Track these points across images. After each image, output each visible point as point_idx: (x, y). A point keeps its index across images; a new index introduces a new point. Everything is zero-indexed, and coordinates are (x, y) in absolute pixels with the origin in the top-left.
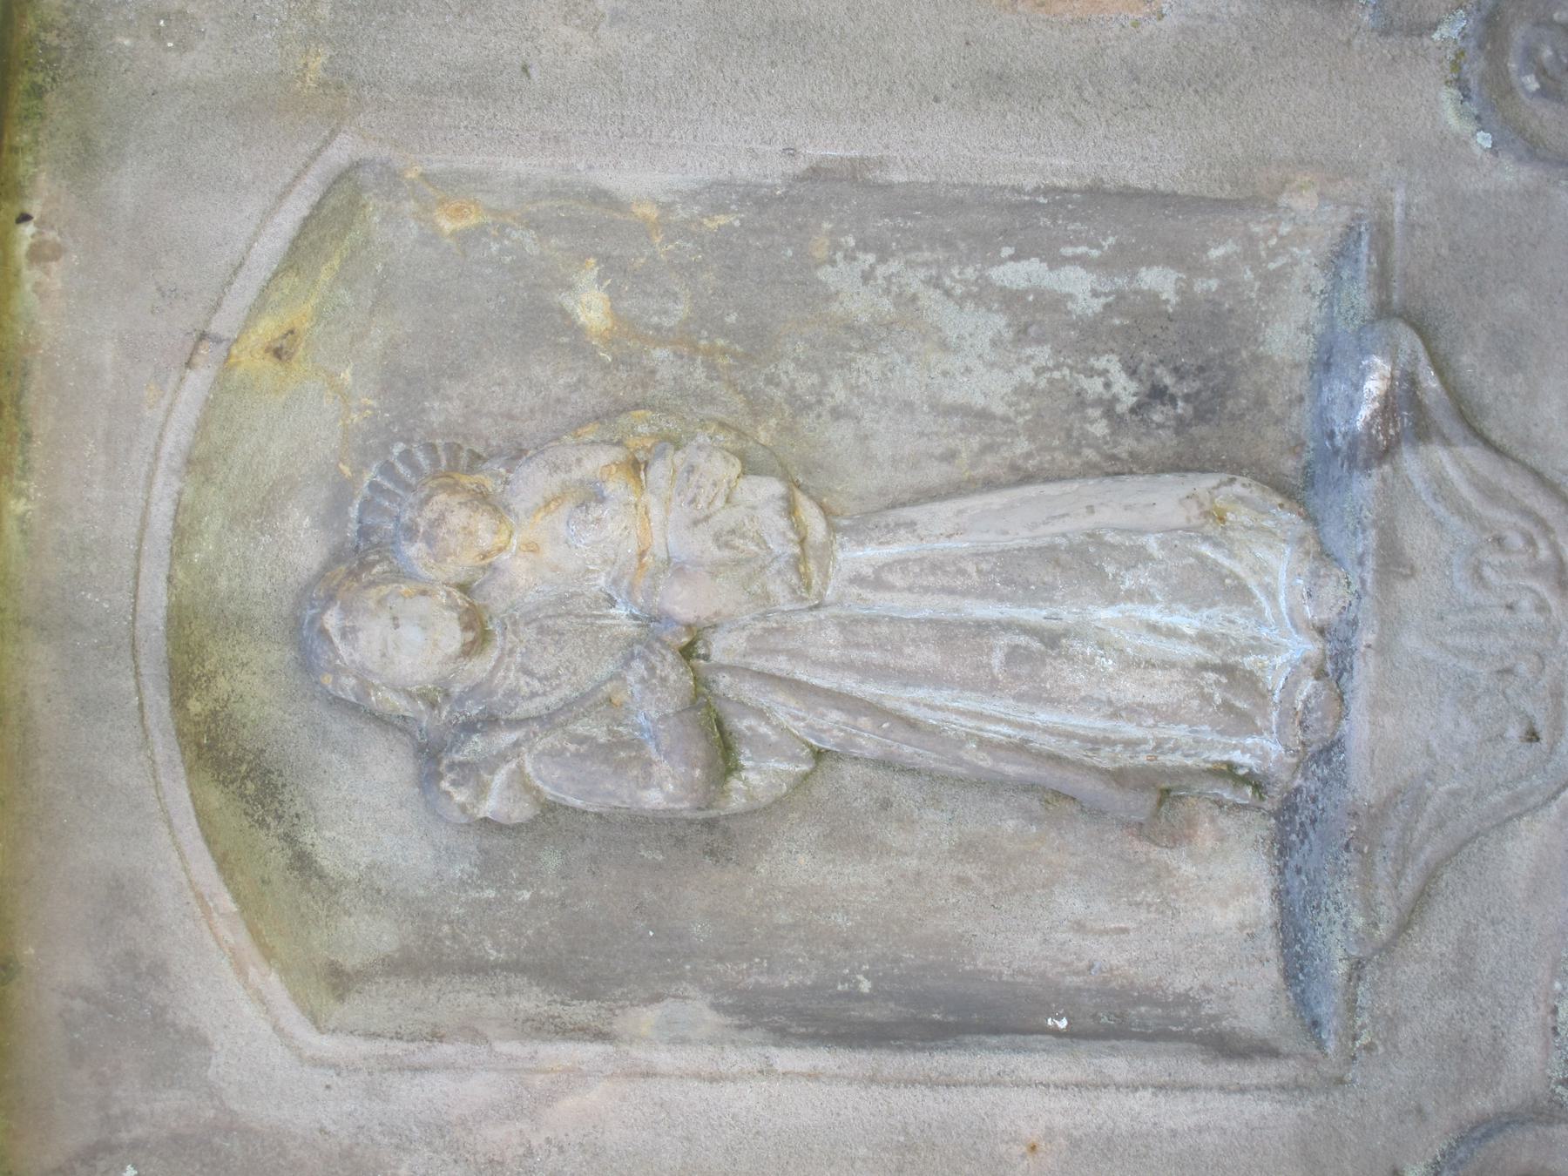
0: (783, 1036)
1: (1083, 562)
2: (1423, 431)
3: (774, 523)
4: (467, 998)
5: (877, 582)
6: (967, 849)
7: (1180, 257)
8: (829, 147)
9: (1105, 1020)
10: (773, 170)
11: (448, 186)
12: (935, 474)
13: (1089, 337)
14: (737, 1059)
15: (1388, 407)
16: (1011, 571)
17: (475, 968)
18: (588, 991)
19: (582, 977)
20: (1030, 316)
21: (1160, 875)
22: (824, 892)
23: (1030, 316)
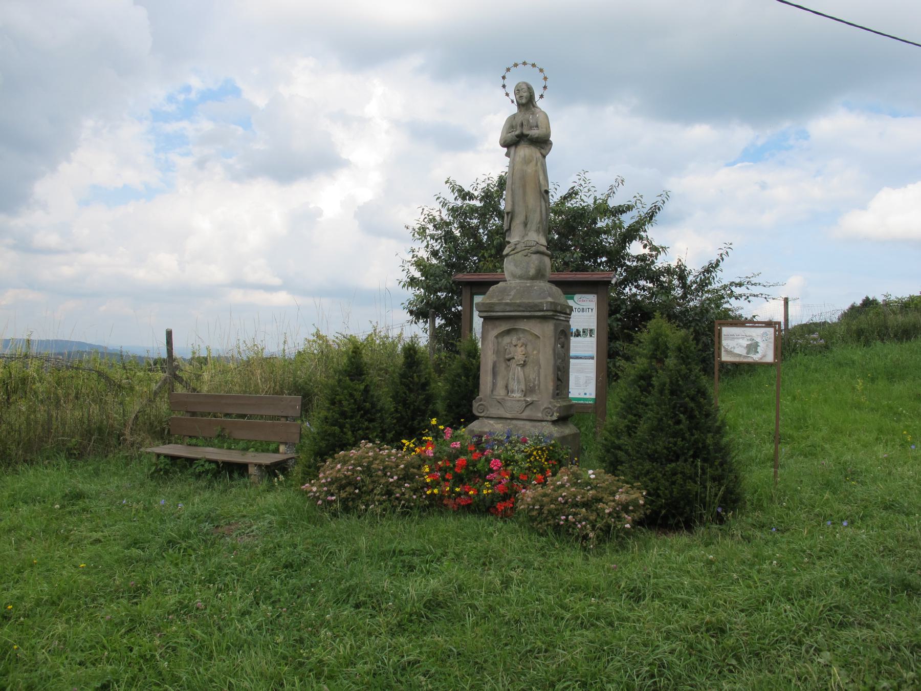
1: (519, 382)
19: (497, 352)
22: (502, 367)
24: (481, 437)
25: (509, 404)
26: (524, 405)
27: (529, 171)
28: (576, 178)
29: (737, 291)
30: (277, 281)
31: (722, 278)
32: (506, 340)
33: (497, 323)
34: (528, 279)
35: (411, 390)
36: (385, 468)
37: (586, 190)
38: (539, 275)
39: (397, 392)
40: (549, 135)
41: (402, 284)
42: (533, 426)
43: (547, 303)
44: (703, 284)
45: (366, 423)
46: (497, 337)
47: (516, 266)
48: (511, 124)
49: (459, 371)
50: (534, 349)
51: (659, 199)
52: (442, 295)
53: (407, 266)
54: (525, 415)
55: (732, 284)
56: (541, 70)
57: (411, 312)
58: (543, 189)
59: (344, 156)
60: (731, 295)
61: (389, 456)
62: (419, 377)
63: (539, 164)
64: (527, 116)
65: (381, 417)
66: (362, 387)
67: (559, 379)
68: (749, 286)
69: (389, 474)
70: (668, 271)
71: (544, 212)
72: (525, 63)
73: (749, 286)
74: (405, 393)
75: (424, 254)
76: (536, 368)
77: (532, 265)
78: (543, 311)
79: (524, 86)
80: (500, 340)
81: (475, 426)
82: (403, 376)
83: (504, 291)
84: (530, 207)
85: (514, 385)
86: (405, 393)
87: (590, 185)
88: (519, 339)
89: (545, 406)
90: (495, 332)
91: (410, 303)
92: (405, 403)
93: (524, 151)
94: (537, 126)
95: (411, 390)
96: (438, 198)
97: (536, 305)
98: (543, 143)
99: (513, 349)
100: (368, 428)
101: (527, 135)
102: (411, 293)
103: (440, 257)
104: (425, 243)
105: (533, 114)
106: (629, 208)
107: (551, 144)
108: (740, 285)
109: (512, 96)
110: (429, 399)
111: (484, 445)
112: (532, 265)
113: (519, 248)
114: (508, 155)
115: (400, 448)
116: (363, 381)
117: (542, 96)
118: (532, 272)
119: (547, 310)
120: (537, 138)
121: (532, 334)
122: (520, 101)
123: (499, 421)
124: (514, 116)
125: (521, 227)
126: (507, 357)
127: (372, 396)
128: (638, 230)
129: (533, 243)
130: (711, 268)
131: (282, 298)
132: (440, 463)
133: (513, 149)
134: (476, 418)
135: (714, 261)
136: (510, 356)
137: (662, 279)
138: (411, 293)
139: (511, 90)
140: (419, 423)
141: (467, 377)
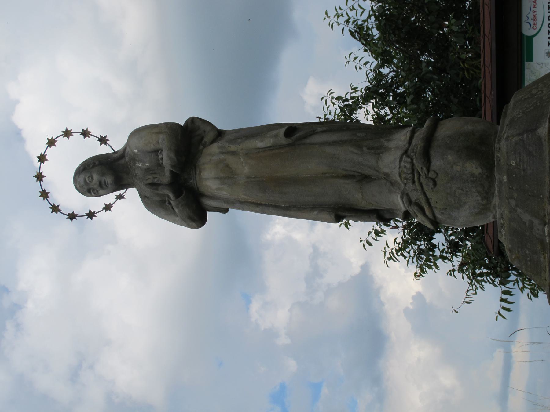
27: (246, 170)
28: (337, 29)
30: (499, 355)
34: (490, 177)
37: (352, 14)
38: (480, 149)
40: (172, 128)
48: (156, 203)
58: (283, 140)
59: (357, 270)
63: (233, 148)
64: (139, 172)
71: (335, 137)
79: (81, 179)
87: (344, 7)
93: (208, 180)
96: (369, 244)
107: (193, 121)
109: (110, 198)
117: (103, 140)
118: (473, 168)
120: (178, 152)
131: (520, 352)
139: (96, 203)
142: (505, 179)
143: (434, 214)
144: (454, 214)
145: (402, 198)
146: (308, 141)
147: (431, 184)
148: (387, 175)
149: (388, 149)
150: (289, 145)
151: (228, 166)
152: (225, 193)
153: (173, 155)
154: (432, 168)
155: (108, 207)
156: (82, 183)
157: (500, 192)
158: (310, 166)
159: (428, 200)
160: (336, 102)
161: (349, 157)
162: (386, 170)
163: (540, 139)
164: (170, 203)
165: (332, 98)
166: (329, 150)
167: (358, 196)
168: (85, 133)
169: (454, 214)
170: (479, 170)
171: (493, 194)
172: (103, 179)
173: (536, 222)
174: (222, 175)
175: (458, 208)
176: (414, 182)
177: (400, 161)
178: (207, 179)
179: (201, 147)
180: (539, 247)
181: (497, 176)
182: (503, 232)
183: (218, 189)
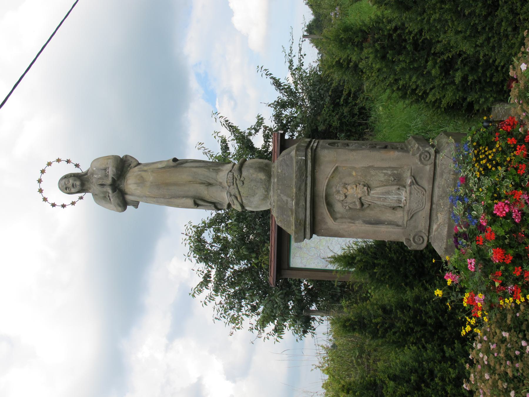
0: (366, 224)
1: (388, 193)
2: (413, 184)
3: (366, 190)
4: (344, 220)
5: (373, 194)
6: (380, 211)
7: (396, 170)
8: (371, 164)
9: (417, 145)
10: (367, 166)
11: (344, 167)
12: (378, 185)
13: (390, 175)
14: (363, 225)
15: (411, 182)
16: (383, 194)
17: (345, 218)
18: (353, 220)
19: (353, 219)
20: (385, 174)
21: (394, 213)
22: (370, 214)
23: (385, 174)
24: (457, 236)
25: (414, 206)
26: (416, 186)
29: (296, 64)
31: (287, 78)
32: (338, 207)
33: (318, 218)
35: (392, 326)
36: (508, 357)
39: (394, 342)
40: (116, 158)
41: (279, 339)
42: (442, 175)
43: (297, 155)
44: (288, 91)
45: (437, 380)
46: (335, 219)
47: (254, 195)
48: (101, 198)
49: (367, 275)
50: (350, 175)
51: (218, 120)
52: (291, 304)
53: (264, 335)
54: (427, 186)
55: (290, 68)
56: (49, 164)
57: (305, 332)
58: (172, 164)
59: (195, 380)
60: (299, 69)
61: (488, 351)
62: (375, 317)
63: (145, 168)
65: (428, 361)
66: (392, 384)
67: (386, 147)
68: (292, 56)
69: (517, 353)
70: (278, 117)
72: (40, 181)
73: (292, 56)
74: (395, 333)
75: (255, 319)
76: (373, 172)
77: (254, 176)
78: (306, 160)
80: (338, 215)
81: (439, 247)
82: (375, 335)
83: (282, 208)
84: (190, 178)
85: (392, 199)
86: (395, 333)
88: (338, 192)
89: (417, 161)
90: (329, 220)
91: (297, 333)
92: (408, 332)
93: (131, 184)
94: (105, 169)
95: (392, 326)
97: (299, 169)
98: (123, 165)
99: (349, 200)
100: (442, 379)
101: (114, 180)
102: (288, 333)
103: (257, 303)
104: (244, 317)
105: (92, 174)
106: (224, 141)
107: (126, 156)
108: (291, 62)
109: (75, 197)
110: (403, 306)
111: (472, 227)
112: (254, 176)
113: (234, 191)
114: (136, 205)
115: (472, 336)
116: (383, 382)
117: (77, 166)
118: (262, 176)
119: (306, 156)
120: (117, 169)
121: (332, 177)
122: (78, 188)
123: (434, 217)
124: (94, 195)
125: (212, 189)
126: (358, 207)
127: (402, 371)
128: (243, 137)
129: (230, 175)
130: (277, 83)
132: (497, 284)
133: (129, 198)
134: (429, 245)
135: (272, 81)
136: (358, 203)
137: (284, 122)
138: (288, 333)
139: (67, 198)
140: (430, 317)
141: (374, 265)
142: (276, 180)
143: (242, 200)
144: (252, 199)
145: (227, 194)
146: (184, 165)
147: (241, 183)
148: (221, 183)
149: (222, 171)
150: (173, 167)
151: (142, 177)
152: (138, 191)
153: (114, 169)
154: (243, 175)
155: (73, 203)
156: (63, 184)
157: (273, 188)
158: (183, 176)
159: (239, 192)
160: (193, 229)
161: (203, 173)
162: (220, 180)
163: (292, 157)
164: (109, 196)
165: (191, 225)
166: (194, 170)
167: (206, 192)
168: (68, 161)
169: (252, 199)
170: (264, 177)
171: (270, 189)
172: (75, 183)
173: (289, 199)
174: (138, 182)
175: (253, 196)
176: (233, 184)
177: (228, 175)
178: (130, 184)
179: (129, 169)
180: (290, 213)
181: (272, 180)
182: (274, 209)
183: (135, 189)
